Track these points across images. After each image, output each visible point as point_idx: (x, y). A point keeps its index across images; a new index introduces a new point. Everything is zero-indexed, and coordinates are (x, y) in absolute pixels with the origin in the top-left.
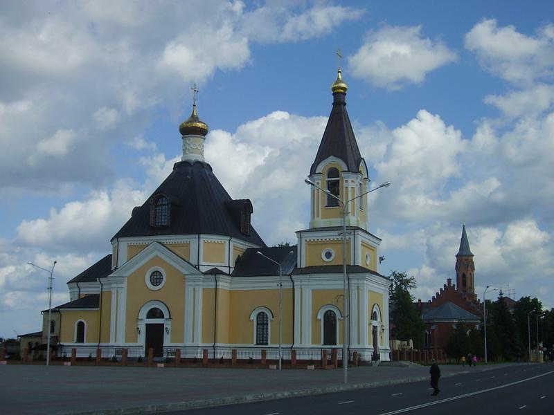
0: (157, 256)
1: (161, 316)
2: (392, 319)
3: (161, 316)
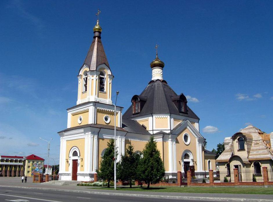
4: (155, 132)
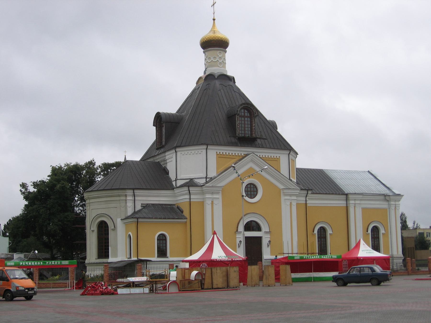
0: (251, 168)
1: (259, 228)
2: (125, 277)
3: (259, 228)
4: (179, 183)
